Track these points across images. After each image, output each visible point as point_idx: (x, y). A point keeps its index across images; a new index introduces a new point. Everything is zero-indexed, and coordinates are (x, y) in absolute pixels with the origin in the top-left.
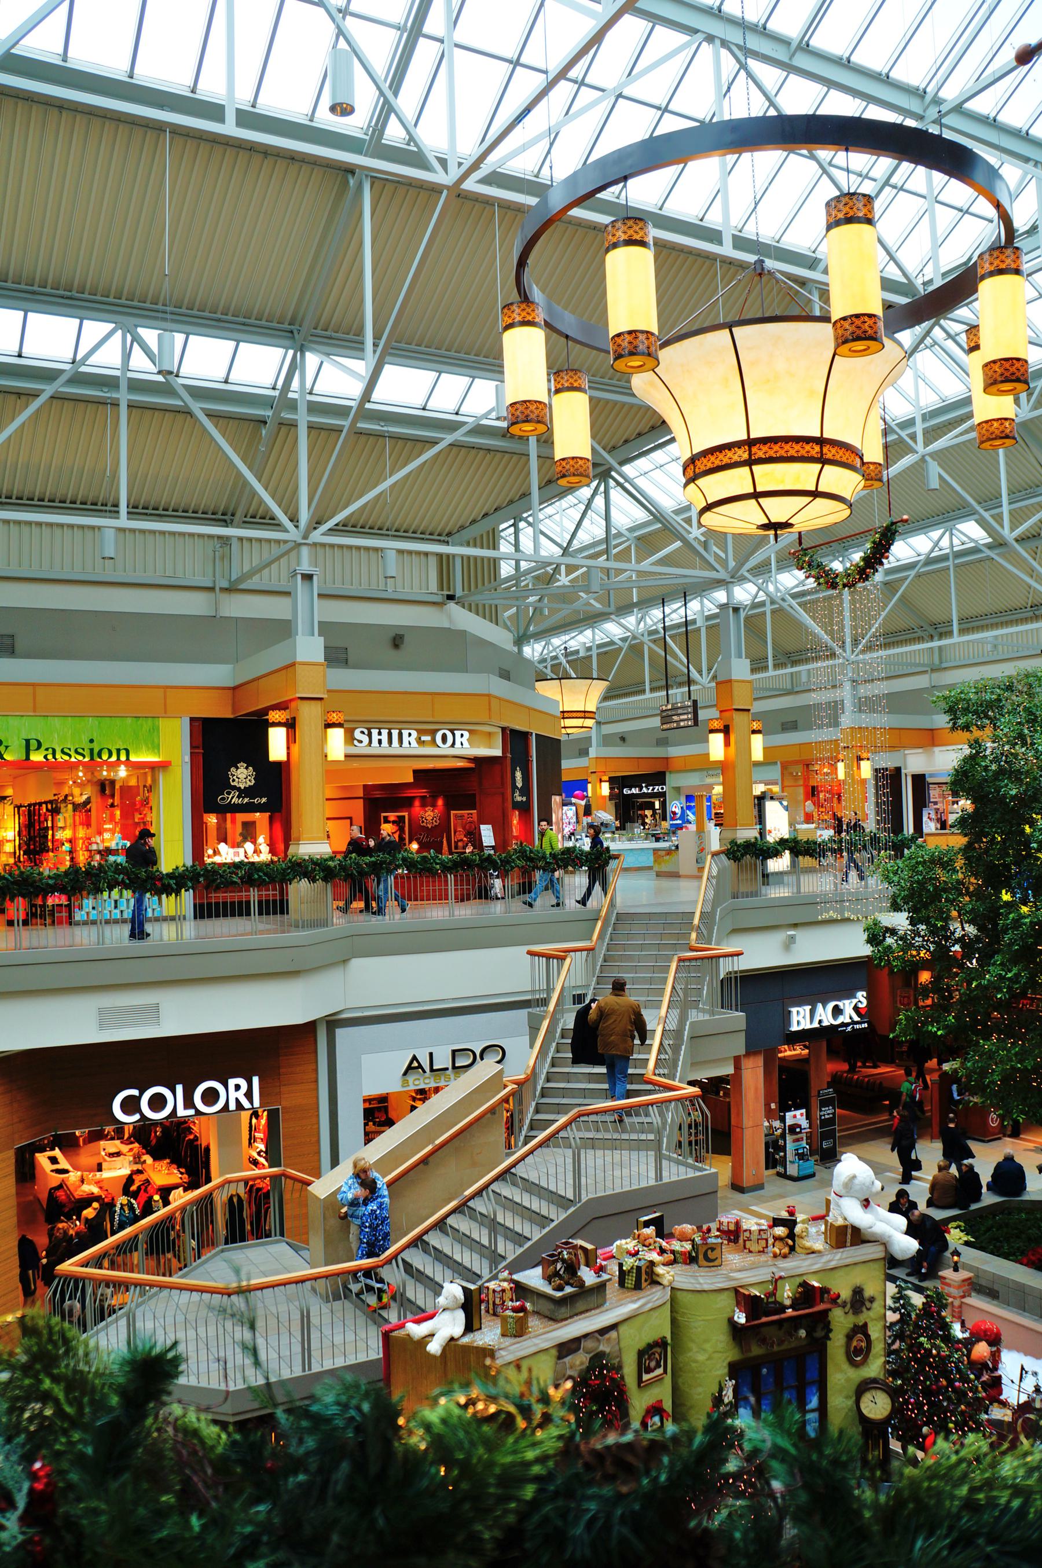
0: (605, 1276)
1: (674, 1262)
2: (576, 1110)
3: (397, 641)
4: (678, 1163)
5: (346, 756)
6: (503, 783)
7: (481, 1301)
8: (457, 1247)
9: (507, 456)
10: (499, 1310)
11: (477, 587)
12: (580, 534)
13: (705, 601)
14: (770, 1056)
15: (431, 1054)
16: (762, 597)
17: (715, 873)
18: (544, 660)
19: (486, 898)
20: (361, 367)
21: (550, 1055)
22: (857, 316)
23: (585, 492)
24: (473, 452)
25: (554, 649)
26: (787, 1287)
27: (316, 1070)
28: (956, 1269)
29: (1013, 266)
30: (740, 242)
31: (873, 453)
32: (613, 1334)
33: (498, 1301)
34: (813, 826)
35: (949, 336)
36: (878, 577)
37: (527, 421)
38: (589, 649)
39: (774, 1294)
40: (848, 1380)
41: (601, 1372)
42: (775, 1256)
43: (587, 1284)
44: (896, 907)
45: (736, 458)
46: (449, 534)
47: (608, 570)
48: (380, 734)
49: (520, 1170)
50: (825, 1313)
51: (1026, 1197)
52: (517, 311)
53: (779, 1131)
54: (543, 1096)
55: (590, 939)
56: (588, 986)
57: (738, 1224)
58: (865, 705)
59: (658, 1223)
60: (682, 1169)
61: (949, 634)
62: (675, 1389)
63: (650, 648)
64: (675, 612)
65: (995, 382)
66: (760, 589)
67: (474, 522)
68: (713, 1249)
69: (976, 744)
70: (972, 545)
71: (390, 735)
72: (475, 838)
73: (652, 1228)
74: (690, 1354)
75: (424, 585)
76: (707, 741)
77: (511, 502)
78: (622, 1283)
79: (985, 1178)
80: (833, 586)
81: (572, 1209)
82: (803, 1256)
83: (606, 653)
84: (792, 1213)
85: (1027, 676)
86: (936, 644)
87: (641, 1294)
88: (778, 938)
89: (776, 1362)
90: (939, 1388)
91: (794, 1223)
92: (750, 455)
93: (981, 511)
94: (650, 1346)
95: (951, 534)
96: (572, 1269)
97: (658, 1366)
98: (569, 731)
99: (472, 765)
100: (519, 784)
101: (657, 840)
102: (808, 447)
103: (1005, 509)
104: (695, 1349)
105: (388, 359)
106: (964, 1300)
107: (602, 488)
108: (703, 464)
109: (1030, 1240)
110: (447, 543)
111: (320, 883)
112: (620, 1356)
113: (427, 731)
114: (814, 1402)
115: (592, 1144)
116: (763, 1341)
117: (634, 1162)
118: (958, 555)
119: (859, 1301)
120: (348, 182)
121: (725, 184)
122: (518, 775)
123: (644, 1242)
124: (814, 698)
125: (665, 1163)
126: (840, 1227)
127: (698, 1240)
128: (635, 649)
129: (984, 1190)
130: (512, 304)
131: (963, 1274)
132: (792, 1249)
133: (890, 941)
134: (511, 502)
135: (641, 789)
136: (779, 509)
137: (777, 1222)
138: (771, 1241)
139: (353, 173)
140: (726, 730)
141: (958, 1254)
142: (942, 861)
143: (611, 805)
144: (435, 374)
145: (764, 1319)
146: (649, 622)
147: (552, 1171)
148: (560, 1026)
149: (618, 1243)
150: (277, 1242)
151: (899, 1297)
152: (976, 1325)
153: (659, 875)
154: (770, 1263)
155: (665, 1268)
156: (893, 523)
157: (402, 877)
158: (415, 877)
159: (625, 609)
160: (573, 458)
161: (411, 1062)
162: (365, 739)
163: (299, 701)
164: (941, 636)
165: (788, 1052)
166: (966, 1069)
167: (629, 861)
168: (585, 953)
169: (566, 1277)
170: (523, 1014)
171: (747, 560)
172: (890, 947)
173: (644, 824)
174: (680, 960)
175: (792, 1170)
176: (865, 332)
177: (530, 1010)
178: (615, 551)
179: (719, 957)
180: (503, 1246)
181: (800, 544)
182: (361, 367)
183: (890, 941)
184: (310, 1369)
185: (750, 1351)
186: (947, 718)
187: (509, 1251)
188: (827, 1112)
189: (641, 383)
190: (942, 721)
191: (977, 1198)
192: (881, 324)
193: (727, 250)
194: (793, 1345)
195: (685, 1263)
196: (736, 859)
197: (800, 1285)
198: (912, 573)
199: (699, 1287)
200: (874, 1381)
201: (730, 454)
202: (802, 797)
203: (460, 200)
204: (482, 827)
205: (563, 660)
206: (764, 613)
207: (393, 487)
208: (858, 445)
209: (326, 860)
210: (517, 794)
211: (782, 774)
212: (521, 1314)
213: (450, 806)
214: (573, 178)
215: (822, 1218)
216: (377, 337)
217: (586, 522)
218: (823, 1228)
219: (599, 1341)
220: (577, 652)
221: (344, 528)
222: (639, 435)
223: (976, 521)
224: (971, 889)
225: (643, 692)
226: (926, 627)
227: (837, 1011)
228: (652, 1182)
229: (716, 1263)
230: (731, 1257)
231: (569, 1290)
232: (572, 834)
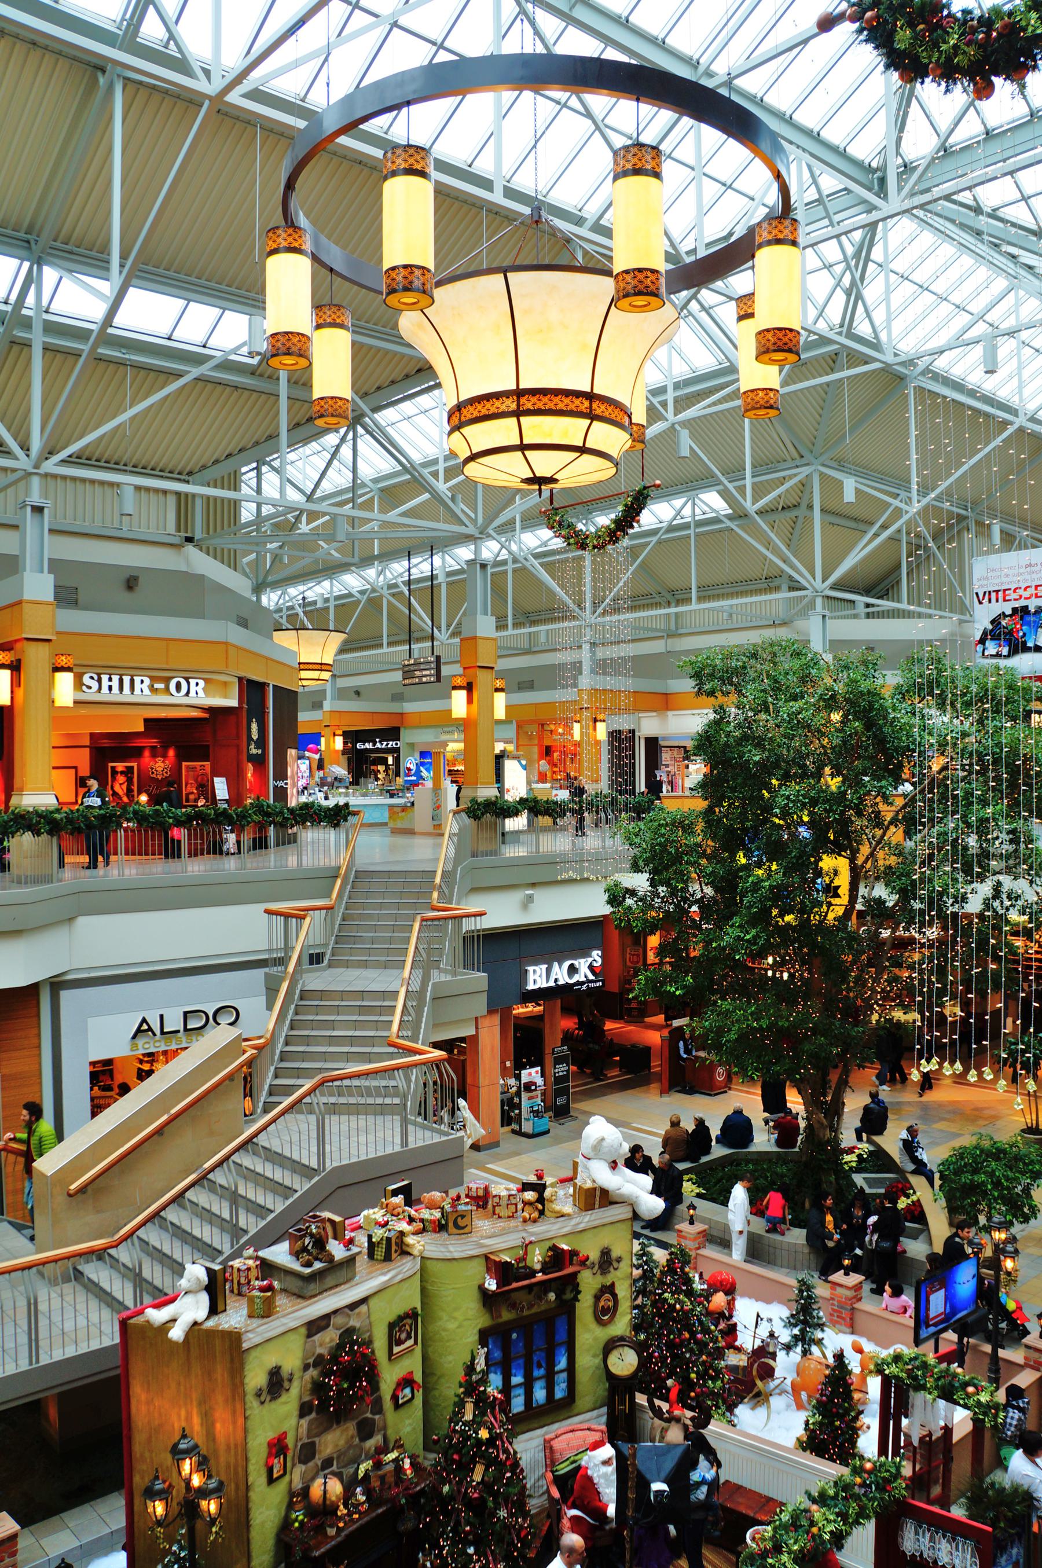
0: (355, 1250)
1: (424, 1230)
2: (320, 1077)
3: (131, 583)
4: (424, 1127)
5: (75, 702)
6: (238, 736)
7: (226, 1280)
8: (197, 1222)
9: (255, 395)
10: (245, 1289)
11: (215, 530)
12: (325, 484)
13: (447, 557)
14: (505, 1014)
15: (162, 1016)
16: (504, 555)
17: (456, 830)
18: (280, 610)
19: (221, 853)
20: (106, 288)
21: (289, 1017)
22: (640, 270)
23: (331, 439)
24: (220, 388)
25: (291, 600)
27: (39, 1035)
28: (692, 1223)
29: (790, 237)
30: (510, 193)
31: (639, 416)
32: (363, 1308)
33: (243, 1280)
34: (548, 785)
35: (703, 308)
36: (625, 542)
37: (289, 354)
38: (327, 600)
39: (525, 1259)
40: (596, 1339)
41: (352, 1348)
42: (525, 1221)
44: (636, 868)
45: (503, 408)
46: (190, 473)
47: (353, 518)
48: (110, 680)
49: (262, 1140)
50: (574, 1275)
51: (753, 1149)
52: (284, 235)
53: (514, 1089)
54: (282, 1060)
55: (329, 896)
56: (326, 945)
57: (486, 1189)
58: (602, 667)
60: (428, 1134)
61: (689, 600)
62: (425, 1358)
63: (389, 602)
64: (421, 567)
65: (767, 351)
66: (503, 547)
67: (216, 462)
68: (463, 1217)
69: (721, 710)
70: (713, 515)
71: (121, 681)
72: (206, 790)
73: (401, 1197)
74: (439, 1323)
75: (161, 524)
76: (450, 697)
77: (257, 443)
78: (371, 1255)
79: (715, 1131)
80: (583, 546)
81: (316, 1179)
82: (553, 1220)
83: (343, 605)
84: (540, 1177)
85: (771, 645)
86: (673, 610)
87: (391, 1265)
88: (516, 897)
89: (525, 1326)
90: (683, 1341)
91: (544, 1187)
92: (518, 405)
93: (726, 482)
94: (401, 1318)
95: (694, 504)
96: (320, 1243)
97: (409, 1337)
98: (305, 683)
99: (206, 716)
100: (255, 736)
101: (392, 796)
102: (577, 402)
103: (748, 482)
104: (445, 1318)
105: (134, 281)
107: (350, 435)
108: (469, 413)
110: (188, 482)
111: (45, 837)
112: (370, 1330)
113: (161, 678)
114: (562, 1363)
115: (334, 1109)
116: (513, 1306)
117: (380, 1128)
118: (700, 524)
119: (606, 1261)
120: (97, 81)
121: (499, 127)
122: (254, 726)
123: (392, 1211)
124: (559, 658)
125: (411, 1128)
126: (588, 1190)
127: (448, 1208)
128: (373, 601)
129: (713, 1143)
130: (277, 228)
131: (699, 1227)
132: (542, 1213)
133: (629, 901)
134: (257, 443)
135: (375, 744)
136: (544, 464)
137: (526, 1187)
138: (520, 1206)
139: (103, 71)
140: (469, 688)
141: (694, 1208)
142: (684, 825)
143: (344, 760)
144: (183, 302)
145: (515, 1285)
146: (389, 575)
147: (295, 1138)
148: (299, 986)
149: (365, 1213)
151: (644, 1253)
152: (713, 1276)
153: (396, 831)
156: (645, 488)
157: (133, 831)
158: (146, 831)
159: (367, 561)
160: (332, 398)
161: (141, 1025)
162: (95, 685)
163: (25, 643)
164: (679, 602)
165: (520, 1010)
166: (703, 1027)
167: (368, 817)
168: (324, 912)
169: (314, 1252)
170: (259, 974)
171: (497, 516)
172: (630, 908)
173: (377, 779)
174: (423, 920)
175: (527, 1127)
176: (647, 287)
177: (267, 970)
178: (360, 501)
179: (462, 917)
181: (552, 503)
182: (106, 288)
183: (629, 901)
184: (37, 1361)
185: (500, 1316)
186: (692, 683)
187: (251, 1224)
188: (562, 1069)
189: (409, 323)
190: (688, 685)
191: (707, 1151)
192: (663, 281)
193: (497, 197)
194: (543, 1308)
195: (435, 1231)
196: (476, 818)
197: (550, 1249)
198: (654, 539)
199: (449, 1256)
200: (622, 1339)
201: (497, 403)
202: (536, 756)
203: (221, 116)
204: (216, 780)
205: (300, 611)
206: (506, 572)
207: (132, 419)
208: (628, 404)
209: (52, 812)
210: (252, 746)
211: (518, 733)
213: (181, 757)
214: (348, 100)
215: (570, 1179)
216: (124, 257)
217: (330, 472)
218: (571, 1190)
219: (349, 1316)
220: (315, 603)
221: (76, 460)
222: (393, 382)
223: (719, 492)
224: (709, 851)
225: (381, 645)
226: (664, 593)
227: (573, 970)
228: (398, 1148)
229: (466, 1230)
231: (318, 1265)
232: (305, 788)
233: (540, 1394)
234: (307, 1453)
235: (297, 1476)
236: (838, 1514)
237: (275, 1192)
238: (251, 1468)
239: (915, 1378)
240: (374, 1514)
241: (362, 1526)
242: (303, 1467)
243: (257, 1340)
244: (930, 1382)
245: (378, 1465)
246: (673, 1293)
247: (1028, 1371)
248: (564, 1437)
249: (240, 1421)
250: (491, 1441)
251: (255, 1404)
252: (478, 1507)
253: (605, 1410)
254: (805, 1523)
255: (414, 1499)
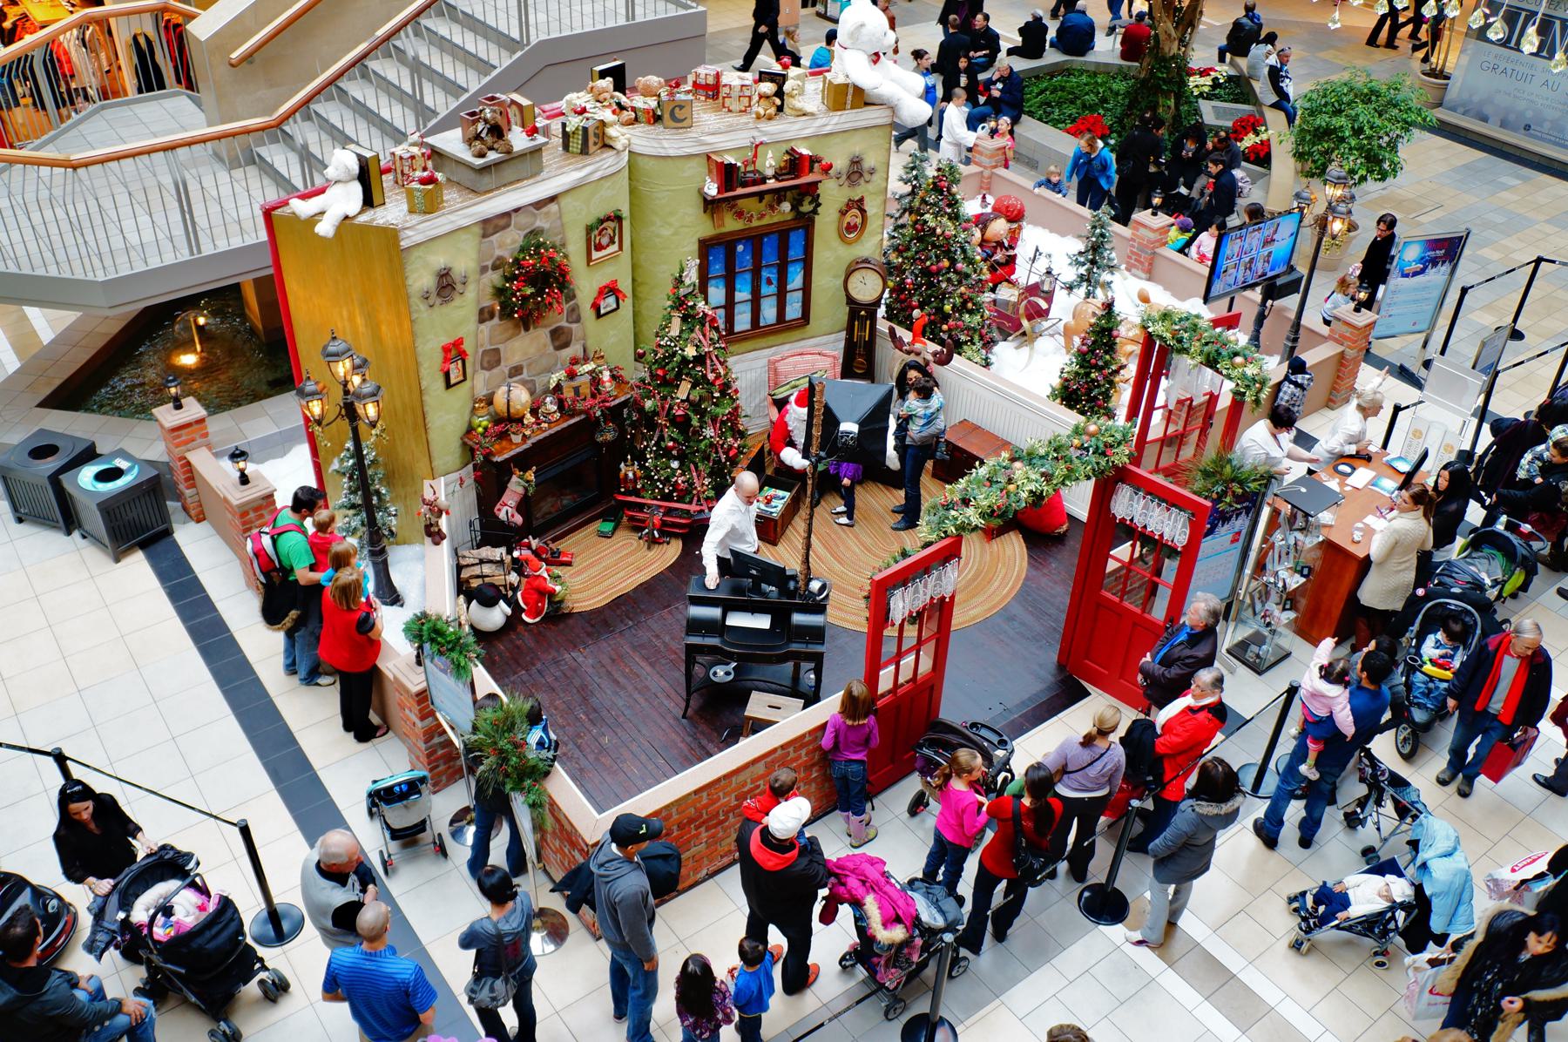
0: (540, 139)
8: (384, 99)
26: (770, 154)
32: (553, 207)
39: (754, 162)
42: (759, 117)
43: (515, 149)
50: (815, 185)
59: (619, 77)
68: (681, 107)
73: (609, 79)
78: (566, 147)
81: (519, 54)
82: (792, 119)
87: (589, 160)
89: (755, 239)
96: (497, 131)
97: (612, 241)
106: (995, 171)
109: (1084, 106)
116: (740, 215)
119: (856, 171)
129: (1047, 44)
132: (780, 109)
138: (756, 98)
145: (740, 191)
149: (568, 97)
150: (174, 95)
154: (751, 125)
155: (625, 130)
169: (489, 139)
180: (434, 98)
185: (723, 225)
194: (775, 220)
195: (649, 122)
200: (866, 261)
212: (430, 187)
219: (535, 216)
228: (622, 21)
230: (705, 116)
231: (492, 156)
233: (769, 313)
234: (492, 359)
235: (480, 382)
236: (1043, 475)
237: (467, 65)
238: (424, 372)
239: (1180, 341)
240: (565, 425)
241: (551, 435)
242: (487, 374)
243: (419, 238)
244: (1195, 347)
245: (572, 375)
246: (936, 215)
247: (1330, 344)
248: (791, 359)
249: (406, 324)
250: (700, 360)
251: (423, 307)
252: (682, 424)
253: (843, 334)
254: (1003, 479)
255: (614, 414)
